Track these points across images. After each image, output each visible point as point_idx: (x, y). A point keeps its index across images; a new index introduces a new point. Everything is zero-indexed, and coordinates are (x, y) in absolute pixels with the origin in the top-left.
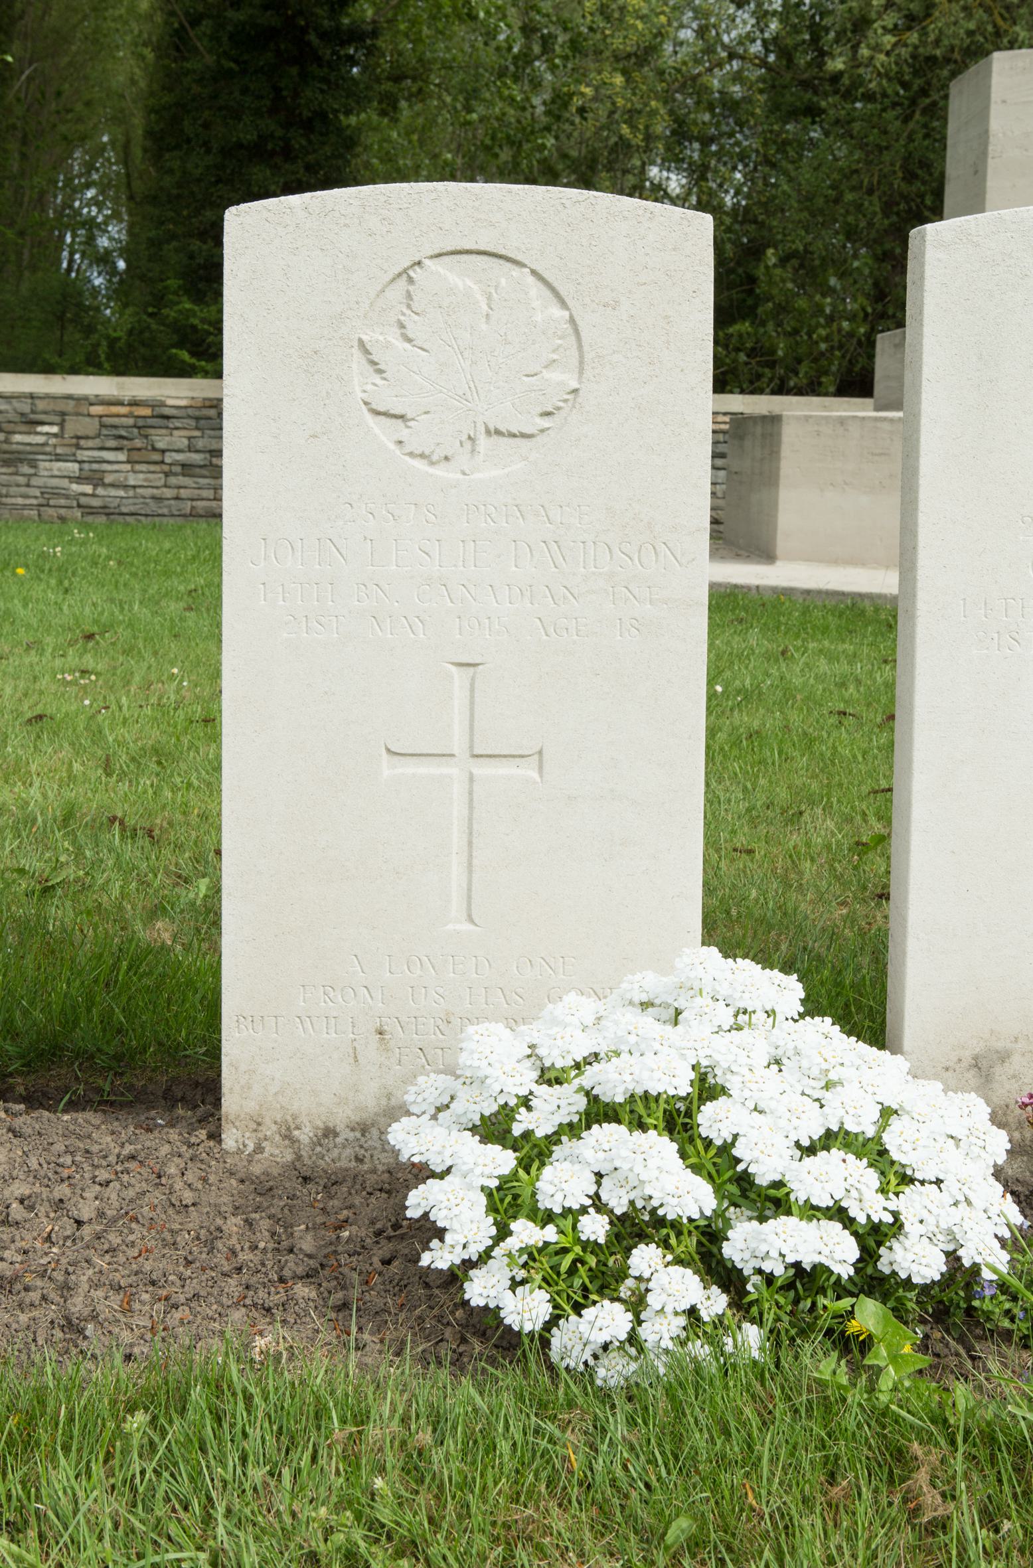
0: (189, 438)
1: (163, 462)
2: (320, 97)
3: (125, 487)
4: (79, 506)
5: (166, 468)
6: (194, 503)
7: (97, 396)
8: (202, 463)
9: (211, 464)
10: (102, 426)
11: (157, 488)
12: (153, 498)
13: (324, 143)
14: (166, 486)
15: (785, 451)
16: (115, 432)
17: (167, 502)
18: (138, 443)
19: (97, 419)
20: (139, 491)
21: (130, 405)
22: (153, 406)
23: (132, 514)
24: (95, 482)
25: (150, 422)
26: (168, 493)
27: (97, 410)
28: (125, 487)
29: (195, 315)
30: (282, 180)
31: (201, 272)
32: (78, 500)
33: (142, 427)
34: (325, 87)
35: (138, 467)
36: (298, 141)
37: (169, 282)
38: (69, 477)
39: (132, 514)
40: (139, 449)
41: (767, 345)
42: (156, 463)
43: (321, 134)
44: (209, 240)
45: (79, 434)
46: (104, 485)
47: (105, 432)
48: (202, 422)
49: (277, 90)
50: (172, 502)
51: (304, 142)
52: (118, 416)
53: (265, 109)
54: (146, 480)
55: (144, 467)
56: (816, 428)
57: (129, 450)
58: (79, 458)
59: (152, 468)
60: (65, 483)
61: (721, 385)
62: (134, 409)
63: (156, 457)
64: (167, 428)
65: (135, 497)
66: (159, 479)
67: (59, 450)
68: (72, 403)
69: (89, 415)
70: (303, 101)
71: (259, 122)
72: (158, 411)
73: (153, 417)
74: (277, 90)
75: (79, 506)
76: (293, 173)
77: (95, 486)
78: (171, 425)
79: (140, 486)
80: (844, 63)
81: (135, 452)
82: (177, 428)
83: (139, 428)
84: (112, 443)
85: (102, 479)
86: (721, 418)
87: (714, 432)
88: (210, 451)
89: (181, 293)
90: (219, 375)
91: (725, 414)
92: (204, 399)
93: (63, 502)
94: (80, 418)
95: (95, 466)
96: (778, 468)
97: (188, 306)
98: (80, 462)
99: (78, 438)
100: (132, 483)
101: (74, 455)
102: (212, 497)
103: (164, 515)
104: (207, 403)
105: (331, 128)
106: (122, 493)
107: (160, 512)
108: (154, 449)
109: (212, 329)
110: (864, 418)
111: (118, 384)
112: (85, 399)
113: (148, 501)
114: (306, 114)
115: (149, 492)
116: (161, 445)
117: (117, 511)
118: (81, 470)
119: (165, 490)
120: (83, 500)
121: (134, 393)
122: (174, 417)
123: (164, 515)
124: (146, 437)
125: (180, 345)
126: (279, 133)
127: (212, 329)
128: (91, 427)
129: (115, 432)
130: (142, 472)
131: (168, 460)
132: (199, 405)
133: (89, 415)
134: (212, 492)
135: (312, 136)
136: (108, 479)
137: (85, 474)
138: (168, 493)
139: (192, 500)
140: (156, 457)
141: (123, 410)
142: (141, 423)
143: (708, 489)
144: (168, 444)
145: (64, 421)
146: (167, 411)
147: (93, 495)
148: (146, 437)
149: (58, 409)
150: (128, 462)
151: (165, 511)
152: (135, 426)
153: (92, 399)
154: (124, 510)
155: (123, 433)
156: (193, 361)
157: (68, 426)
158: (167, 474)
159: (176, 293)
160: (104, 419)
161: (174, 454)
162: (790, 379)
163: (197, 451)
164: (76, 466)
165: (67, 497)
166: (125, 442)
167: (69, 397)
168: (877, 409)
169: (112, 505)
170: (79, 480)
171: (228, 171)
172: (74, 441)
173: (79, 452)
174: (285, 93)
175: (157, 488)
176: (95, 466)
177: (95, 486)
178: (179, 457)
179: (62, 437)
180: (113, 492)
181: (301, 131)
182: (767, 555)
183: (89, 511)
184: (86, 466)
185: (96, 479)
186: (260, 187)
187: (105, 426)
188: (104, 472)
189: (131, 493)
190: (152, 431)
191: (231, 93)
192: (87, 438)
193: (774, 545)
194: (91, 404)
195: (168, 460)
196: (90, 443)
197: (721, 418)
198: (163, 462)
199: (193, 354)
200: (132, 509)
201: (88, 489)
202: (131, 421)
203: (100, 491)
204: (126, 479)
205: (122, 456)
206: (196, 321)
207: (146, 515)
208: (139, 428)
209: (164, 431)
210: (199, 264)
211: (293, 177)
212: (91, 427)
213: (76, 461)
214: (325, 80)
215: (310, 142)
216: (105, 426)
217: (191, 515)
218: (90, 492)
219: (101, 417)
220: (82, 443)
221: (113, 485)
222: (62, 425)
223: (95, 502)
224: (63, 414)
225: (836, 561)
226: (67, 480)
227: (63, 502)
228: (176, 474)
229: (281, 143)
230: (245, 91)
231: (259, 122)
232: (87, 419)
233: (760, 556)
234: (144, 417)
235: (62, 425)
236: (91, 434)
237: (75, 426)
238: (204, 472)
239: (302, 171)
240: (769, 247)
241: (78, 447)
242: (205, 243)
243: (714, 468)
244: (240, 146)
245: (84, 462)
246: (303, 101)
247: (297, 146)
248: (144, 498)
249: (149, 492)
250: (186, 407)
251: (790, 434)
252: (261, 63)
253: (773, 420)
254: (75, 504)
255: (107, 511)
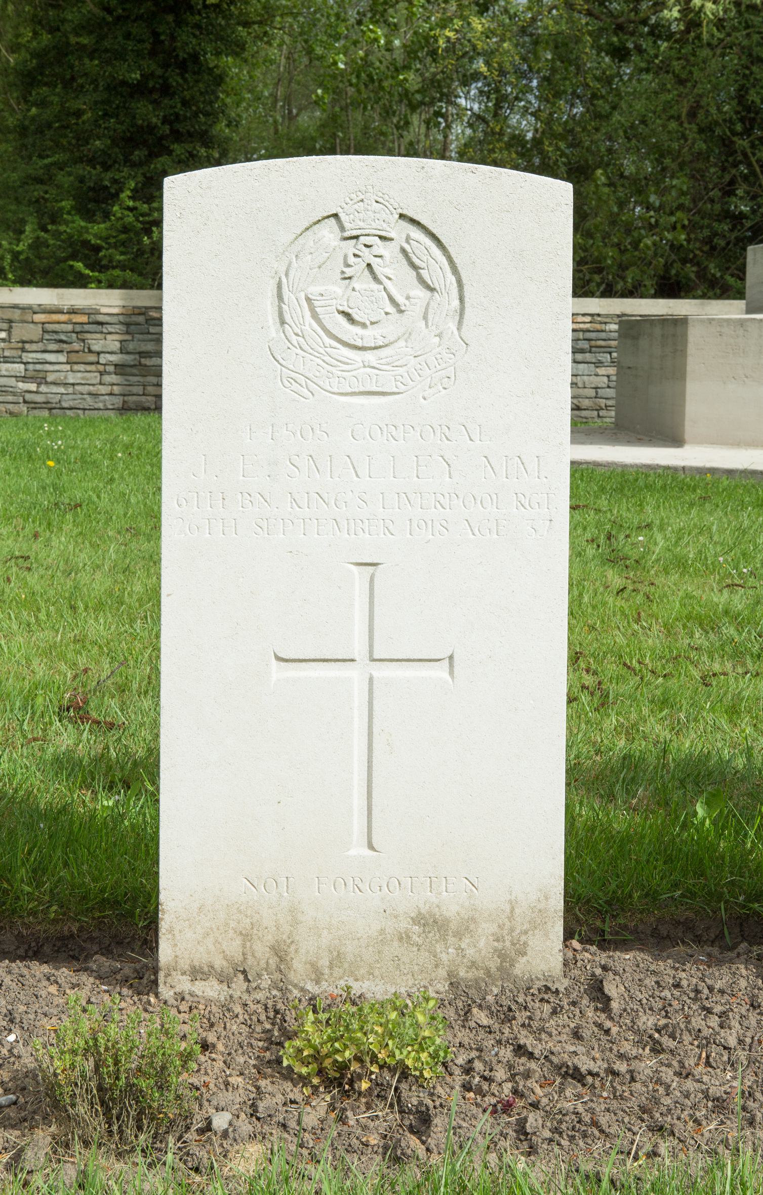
0: (121, 342)
1: (98, 363)
2: (194, 41)
3: (66, 384)
4: (25, 402)
5: (101, 368)
6: (126, 398)
7: (40, 305)
8: (132, 363)
9: (140, 364)
10: (45, 331)
11: (93, 385)
12: (90, 394)
13: (197, 81)
14: (101, 384)
15: (691, 349)
16: (56, 337)
17: (102, 398)
18: (76, 346)
19: (40, 326)
20: (78, 388)
21: (68, 313)
22: (89, 314)
23: (71, 409)
24: (39, 380)
25: (87, 327)
26: (103, 390)
27: (39, 318)
28: (66, 384)
29: (87, 232)
30: (162, 114)
31: (90, 194)
32: (23, 397)
33: (80, 333)
34: (198, 33)
35: (76, 367)
36: (175, 79)
37: (63, 203)
38: (16, 377)
39: (71, 409)
40: (77, 352)
41: (596, 254)
42: (92, 363)
43: (194, 73)
44: (98, 167)
45: (24, 339)
46: (47, 383)
47: (47, 336)
48: (132, 327)
49: (156, 35)
50: (107, 397)
51: (180, 81)
52: (59, 323)
53: (146, 52)
54: (83, 378)
55: (81, 367)
56: (718, 329)
57: (68, 352)
58: (24, 361)
59: (89, 368)
60: (12, 382)
61: (581, 289)
62: (72, 316)
63: (92, 358)
64: (102, 332)
65: (74, 394)
66: (94, 378)
67: (7, 353)
68: (18, 312)
69: (33, 322)
70: (179, 44)
71: (142, 62)
72: (93, 318)
73: (89, 323)
74: (156, 35)
75: (25, 402)
76: (171, 107)
77: (39, 384)
78: (105, 331)
79: (78, 384)
80: (679, 11)
81: (73, 354)
82: (110, 333)
83: (77, 333)
84: (53, 347)
85: (45, 378)
86: (580, 319)
87: (574, 330)
88: (140, 353)
89: (73, 212)
90: (160, 287)
91: (584, 315)
92: (134, 307)
93: (10, 398)
94: (25, 324)
95: (38, 367)
96: (685, 365)
97: (83, 224)
98: (25, 364)
99: (24, 342)
100: (71, 381)
101: (20, 357)
102: (141, 393)
103: (99, 409)
104: (136, 311)
105: (203, 68)
106: (62, 390)
107: (96, 406)
108: (90, 351)
109: (104, 244)
110: (721, 322)
111: (58, 294)
112: (24, 309)
113: (85, 396)
114: (182, 55)
115: (86, 389)
116: (96, 348)
117: (58, 406)
118: (26, 370)
119: (100, 387)
120: (28, 397)
121: (73, 303)
122: (107, 323)
123: (99, 409)
124: (83, 341)
125: (74, 256)
126: (159, 72)
127: (104, 244)
128: (34, 332)
129: (56, 337)
130: (80, 371)
131: (102, 361)
132: (130, 312)
133: (33, 322)
134: (141, 387)
135: (187, 75)
136: (51, 378)
137: (29, 374)
138: (103, 390)
139: (124, 395)
140: (92, 358)
141: (63, 318)
142: (78, 328)
143: (569, 379)
144: (103, 346)
145: (11, 327)
146: (100, 318)
147: (37, 392)
148: (83, 341)
149: (5, 317)
150: (67, 363)
151: (101, 405)
152: (73, 332)
153: (36, 308)
154: (65, 405)
155: (63, 337)
156: (87, 272)
157: (15, 331)
158: (101, 374)
159: (69, 213)
160: (47, 325)
161: (107, 355)
162: (617, 283)
163: (128, 353)
164: (22, 366)
165: (14, 394)
166: (65, 346)
167: (15, 307)
168: (749, 311)
169: (54, 401)
170: (24, 379)
171: (114, 106)
172: (20, 345)
173: (24, 354)
174: (163, 38)
175: (93, 385)
176: (38, 367)
177: (39, 384)
178: (113, 358)
179: (10, 342)
180: (55, 389)
181: (177, 71)
182: (675, 440)
183: (33, 406)
184: (31, 367)
185: (40, 379)
186: (144, 121)
187: (48, 332)
188: (46, 372)
189: (70, 390)
190: (88, 336)
191: (116, 38)
192: (31, 342)
193: (683, 432)
194: (35, 313)
195: (102, 361)
196: (34, 347)
197: (580, 319)
198: (98, 363)
199: (87, 266)
200: (72, 404)
201: (33, 387)
202: (70, 327)
203: (43, 388)
204: (66, 378)
205: (62, 358)
206: (90, 237)
207: (84, 409)
208: (77, 333)
209: (98, 336)
210: (89, 187)
211: (172, 111)
212: (34, 332)
213: (22, 363)
214: (198, 26)
215: (185, 80)
216: (48, 332)
217: (123, 409)
218: (35, 389)
219: (43, 323)
220: (27, 346)
221: (54, 383)
222: (9, 331)
223: (39, 398)
224: (10, 321)
225: (737, 443)
226: (14, 379)
227: (10, 398)
228: (109, 373)
229: (161, 81)
230: (128, 36)
231: (142, 62)
232: (31, 326)
233: (665, 441)
234: (82, 324)
235: (9, 331)
236: (35, 339)
237: (19, 332)
238: (135, 371)
239: (179, 105)
240: (599, 167)
241: (23, 350)
242: (95, 168)
243: (575, 361)
244: (124, 83)
245: (29, 363)
246: (179, 44)
247: (174, 84)
248: (82, 394)
249: (86, 389)
250: (118, 314)
251: (694, 335)
252: (142, 11)
253: (680, 323)
254: (21, 400)
255: (49, 406)
